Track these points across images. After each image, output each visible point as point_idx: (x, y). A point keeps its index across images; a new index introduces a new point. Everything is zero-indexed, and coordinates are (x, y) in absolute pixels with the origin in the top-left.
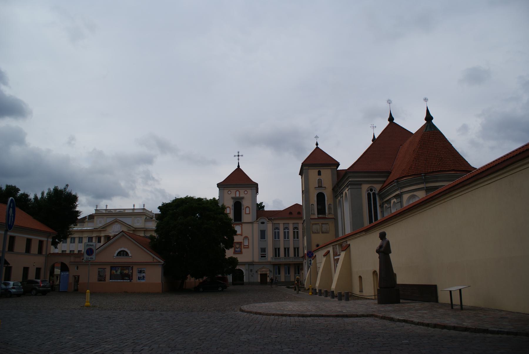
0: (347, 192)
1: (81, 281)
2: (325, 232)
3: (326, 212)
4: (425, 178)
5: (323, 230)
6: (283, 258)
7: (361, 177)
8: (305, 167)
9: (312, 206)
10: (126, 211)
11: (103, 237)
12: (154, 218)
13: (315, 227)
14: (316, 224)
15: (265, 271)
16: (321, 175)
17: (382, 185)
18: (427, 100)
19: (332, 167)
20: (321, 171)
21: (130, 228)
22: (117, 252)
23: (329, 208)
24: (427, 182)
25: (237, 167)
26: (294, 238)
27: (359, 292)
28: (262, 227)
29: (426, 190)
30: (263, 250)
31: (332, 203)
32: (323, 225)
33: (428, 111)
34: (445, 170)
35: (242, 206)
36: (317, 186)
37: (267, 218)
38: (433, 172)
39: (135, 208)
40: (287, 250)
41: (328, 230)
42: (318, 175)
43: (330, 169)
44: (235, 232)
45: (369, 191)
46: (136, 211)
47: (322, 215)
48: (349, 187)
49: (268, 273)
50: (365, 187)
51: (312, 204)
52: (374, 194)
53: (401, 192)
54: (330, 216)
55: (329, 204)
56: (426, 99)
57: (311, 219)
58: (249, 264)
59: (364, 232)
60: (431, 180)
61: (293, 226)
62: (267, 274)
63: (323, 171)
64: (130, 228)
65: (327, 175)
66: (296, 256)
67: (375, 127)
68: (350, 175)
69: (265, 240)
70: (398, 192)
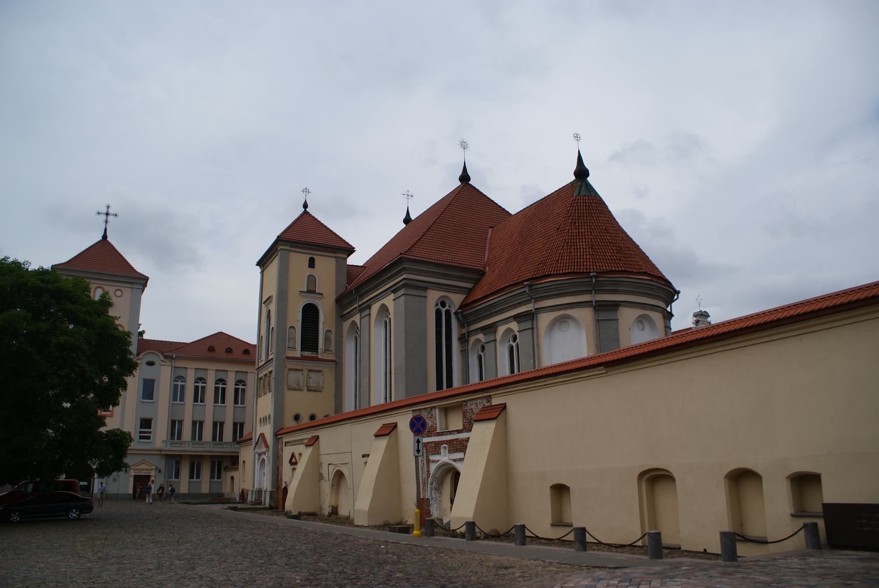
2: (314, 389)
4: (596, 281)
6: (189, 442)
8: (282, 245)
9: (292, 330)
13: (293, 377)
14: (296, 370)
15: (146, 470)
16: (314, 268)
17: (464, 296)
18: (578, 139)
19: (338, 255)
23: (327, 339)
24: (598, 292)
25: (100, 238)
26: (216, 401)
27: (550, 526)
29: (595, 307)
31: (333, 330)
32: (312, 375)
33: (580, 159)
36: (306, 291)
37: (162, 353)
38: (611, 272)
40: (198, 425)
41: (321, 385)
43: (335, 259)
45: (440, 306)
47: (310, 353)
48: (402, 291)
49: (153, 473)
50: (434, 296)
51: (292, 327)
52: (448, 313)
53: (535, 307)
54: (327, 356)
55: (326, 330)
56: (578, 136)
57: (288, 358)
59: (602, 367)
62: (149, 477)
63: (319, 260)
66: (197, 440)
68: (405, 266)
69: (151, 401)
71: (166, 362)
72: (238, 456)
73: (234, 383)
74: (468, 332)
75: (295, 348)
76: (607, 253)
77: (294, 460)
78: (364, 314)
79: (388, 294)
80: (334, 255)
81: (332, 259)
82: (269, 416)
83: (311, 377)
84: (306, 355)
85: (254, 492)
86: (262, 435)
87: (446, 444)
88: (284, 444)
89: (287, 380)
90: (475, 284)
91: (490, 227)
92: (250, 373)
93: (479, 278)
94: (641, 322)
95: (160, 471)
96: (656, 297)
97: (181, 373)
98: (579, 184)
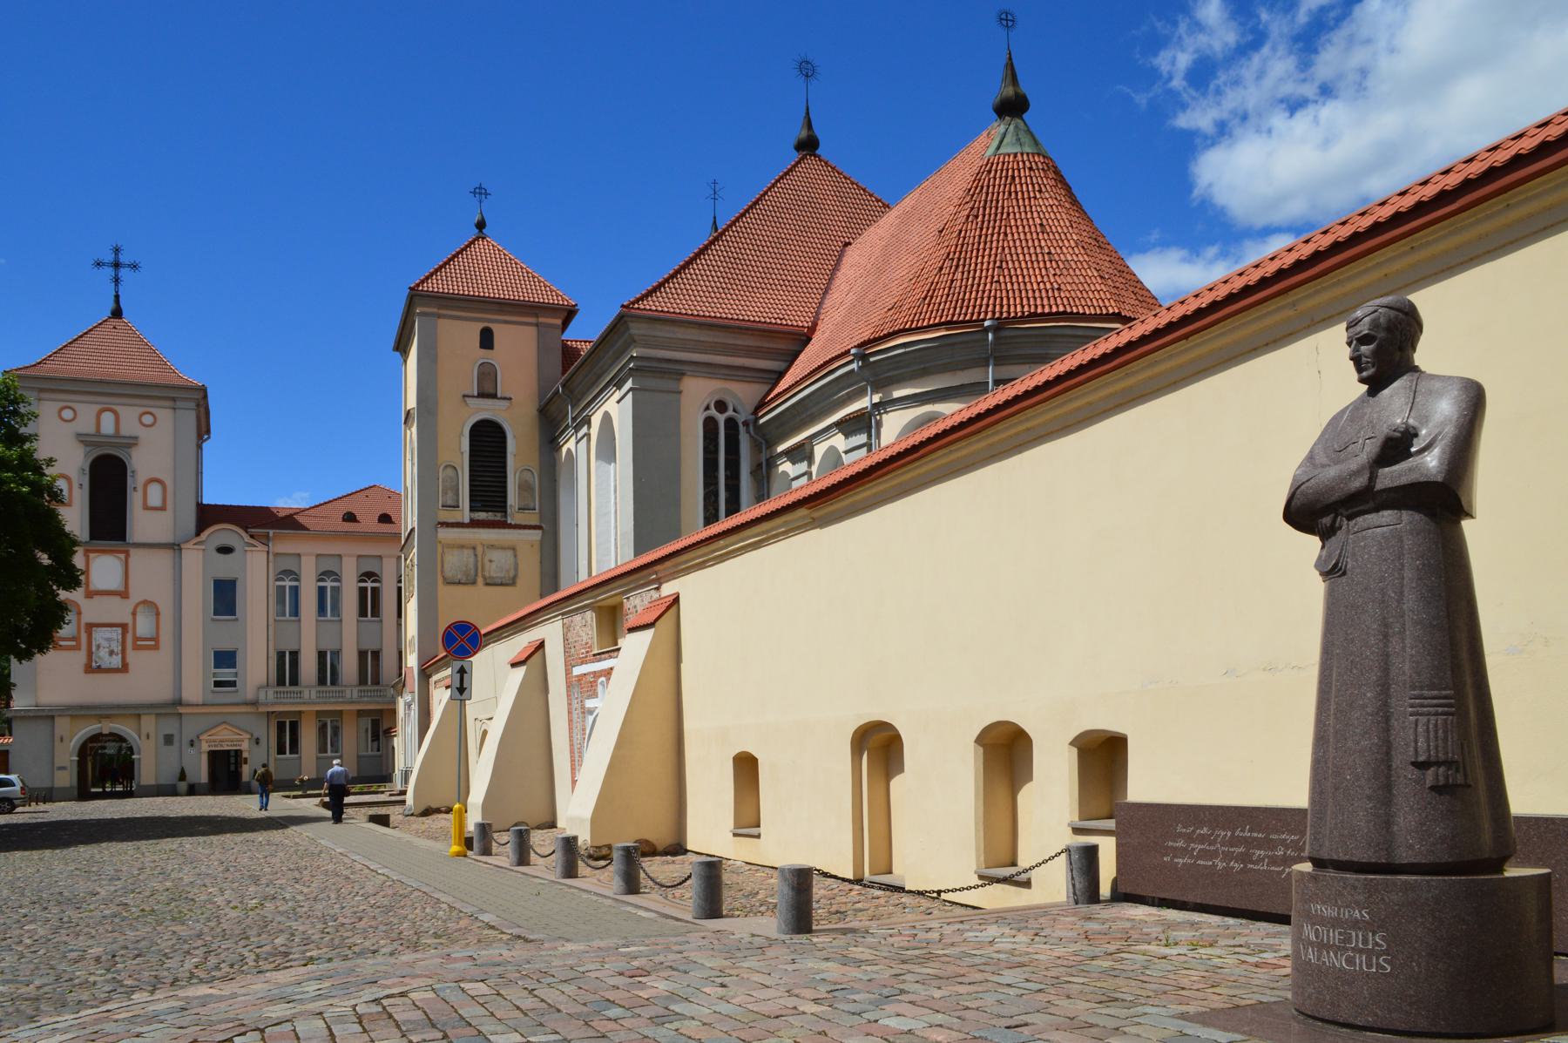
2: (500, 581)
3: (505, 502)
7: (684, 346)
18: (1010, 23)
19: (541, 320)
23: (525, 487)
28: (225, 567)
30: (225, 659)
35: (129, 474)
36: (476, 394)
44: (49, 558)
45: (713, 412)
49: (245, 746)
52: (731, 423)
56: (1010, 17)
58: (157, 715)
63: (500, 332)
66: (369, 683)
70: (863, 403)
71: (255, 546)
72: (395, 709)
73: (313, 577)
75: (458, 507)
76: (1090, 293)
78: (580, 434)
79: (611, 392)
80: (533, 320)
89: (442, 566)
95: (257, 742)
97: (289, 564)
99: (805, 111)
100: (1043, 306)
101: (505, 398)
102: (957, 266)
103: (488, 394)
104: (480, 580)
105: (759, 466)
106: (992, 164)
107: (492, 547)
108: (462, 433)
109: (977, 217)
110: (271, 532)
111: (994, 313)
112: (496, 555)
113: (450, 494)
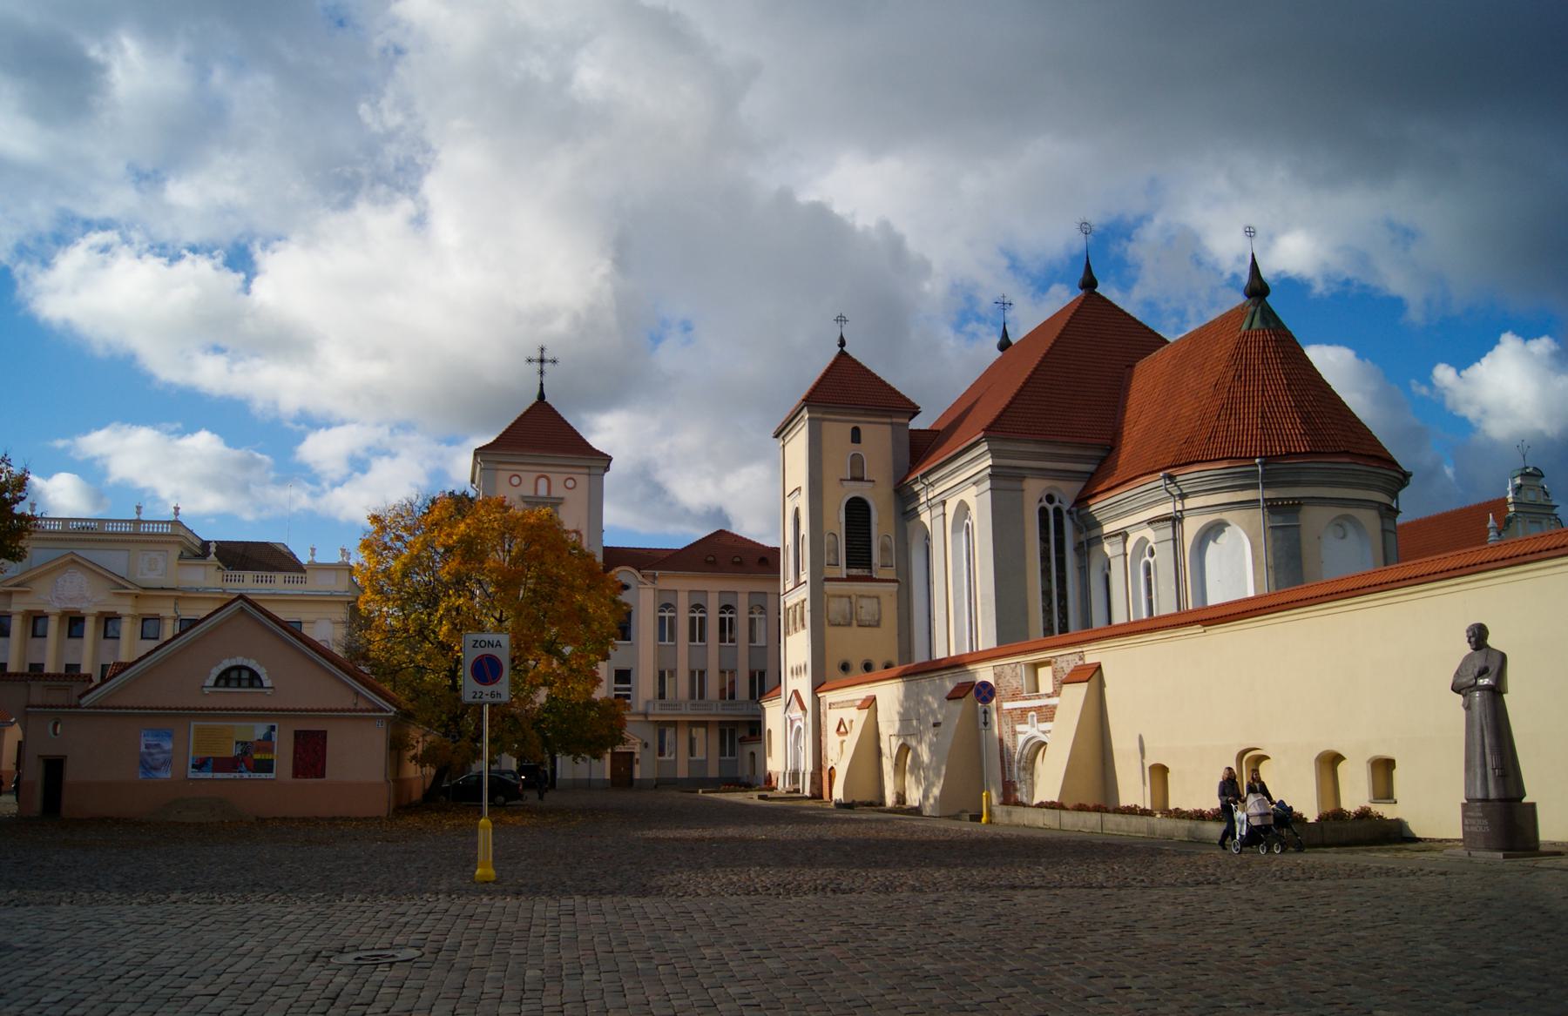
0: (970, 495)
1: (71, 775)
2: (867, 623)
3: (870, 561)
5: (863, 618)
10: (109, 528)
11: (20, 617)
12: (212, 555)
16: (859, 442)
18: (1252, 234)
19: (895, 420)
20: (861, 428)
21: (127, 588)
22: (216, 672)
23: (885, 549)
34: (1324, 453)
36: (845, 576)
39: (143, 517)
42: (853, 442)
45: (1045, 503)
46: (144, 529)
47: (860, 570)
52: (1058, 511)
59: (1199, 626)
60: (1281, 479)
61: (689, 601)
62: (632, 753)
63: (867, 431)
64: (127, 588)
65: (878, 438)
67: (1010, 304)
72: (760, 721)
74: (1087, 540)
77: (842, 729)
80: (888, 420)
81: (886, 426)
82: (805, 666)
83: (863, 605)
84: (854, 574)
85: (787, 775)
86: (796, 692)
87: (1035, 711)
88: (828, 706)
90: (1100, 465)
91: (1127, 366)
92: (771, 593)
93: (1104, 455)
94: (1341, 526)
96: (1368, 487)
97: (668, 599)
98: (1252, 309)
99: (1085, 260)
100: (1295, 447)
101: (870, 481)
102: (1231, 414)
103: (857, 478)
104: (854, 622)
105: (1081, 544)
106: (1248, 337)
107: (862, 596)
108: (840, 508)
109: (1241, 376)
110: (657, 573)
111: (1261, 452)
112: (864, 602)
113: (832, 555)
